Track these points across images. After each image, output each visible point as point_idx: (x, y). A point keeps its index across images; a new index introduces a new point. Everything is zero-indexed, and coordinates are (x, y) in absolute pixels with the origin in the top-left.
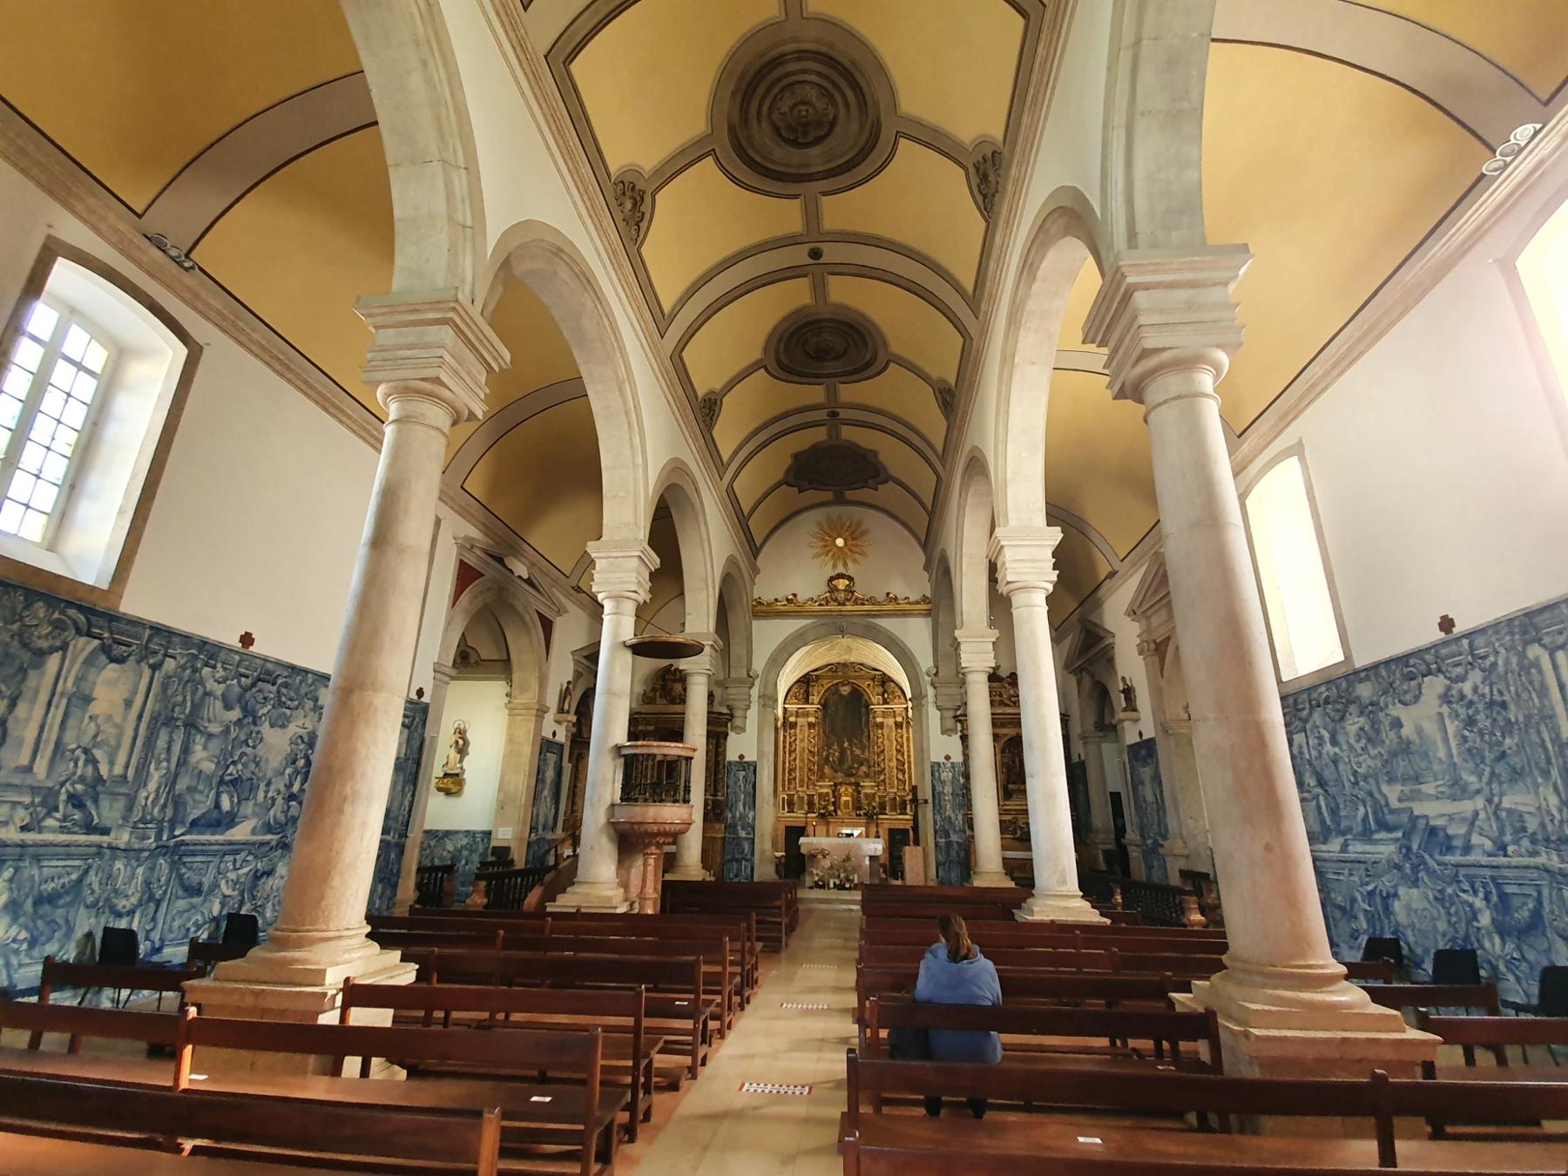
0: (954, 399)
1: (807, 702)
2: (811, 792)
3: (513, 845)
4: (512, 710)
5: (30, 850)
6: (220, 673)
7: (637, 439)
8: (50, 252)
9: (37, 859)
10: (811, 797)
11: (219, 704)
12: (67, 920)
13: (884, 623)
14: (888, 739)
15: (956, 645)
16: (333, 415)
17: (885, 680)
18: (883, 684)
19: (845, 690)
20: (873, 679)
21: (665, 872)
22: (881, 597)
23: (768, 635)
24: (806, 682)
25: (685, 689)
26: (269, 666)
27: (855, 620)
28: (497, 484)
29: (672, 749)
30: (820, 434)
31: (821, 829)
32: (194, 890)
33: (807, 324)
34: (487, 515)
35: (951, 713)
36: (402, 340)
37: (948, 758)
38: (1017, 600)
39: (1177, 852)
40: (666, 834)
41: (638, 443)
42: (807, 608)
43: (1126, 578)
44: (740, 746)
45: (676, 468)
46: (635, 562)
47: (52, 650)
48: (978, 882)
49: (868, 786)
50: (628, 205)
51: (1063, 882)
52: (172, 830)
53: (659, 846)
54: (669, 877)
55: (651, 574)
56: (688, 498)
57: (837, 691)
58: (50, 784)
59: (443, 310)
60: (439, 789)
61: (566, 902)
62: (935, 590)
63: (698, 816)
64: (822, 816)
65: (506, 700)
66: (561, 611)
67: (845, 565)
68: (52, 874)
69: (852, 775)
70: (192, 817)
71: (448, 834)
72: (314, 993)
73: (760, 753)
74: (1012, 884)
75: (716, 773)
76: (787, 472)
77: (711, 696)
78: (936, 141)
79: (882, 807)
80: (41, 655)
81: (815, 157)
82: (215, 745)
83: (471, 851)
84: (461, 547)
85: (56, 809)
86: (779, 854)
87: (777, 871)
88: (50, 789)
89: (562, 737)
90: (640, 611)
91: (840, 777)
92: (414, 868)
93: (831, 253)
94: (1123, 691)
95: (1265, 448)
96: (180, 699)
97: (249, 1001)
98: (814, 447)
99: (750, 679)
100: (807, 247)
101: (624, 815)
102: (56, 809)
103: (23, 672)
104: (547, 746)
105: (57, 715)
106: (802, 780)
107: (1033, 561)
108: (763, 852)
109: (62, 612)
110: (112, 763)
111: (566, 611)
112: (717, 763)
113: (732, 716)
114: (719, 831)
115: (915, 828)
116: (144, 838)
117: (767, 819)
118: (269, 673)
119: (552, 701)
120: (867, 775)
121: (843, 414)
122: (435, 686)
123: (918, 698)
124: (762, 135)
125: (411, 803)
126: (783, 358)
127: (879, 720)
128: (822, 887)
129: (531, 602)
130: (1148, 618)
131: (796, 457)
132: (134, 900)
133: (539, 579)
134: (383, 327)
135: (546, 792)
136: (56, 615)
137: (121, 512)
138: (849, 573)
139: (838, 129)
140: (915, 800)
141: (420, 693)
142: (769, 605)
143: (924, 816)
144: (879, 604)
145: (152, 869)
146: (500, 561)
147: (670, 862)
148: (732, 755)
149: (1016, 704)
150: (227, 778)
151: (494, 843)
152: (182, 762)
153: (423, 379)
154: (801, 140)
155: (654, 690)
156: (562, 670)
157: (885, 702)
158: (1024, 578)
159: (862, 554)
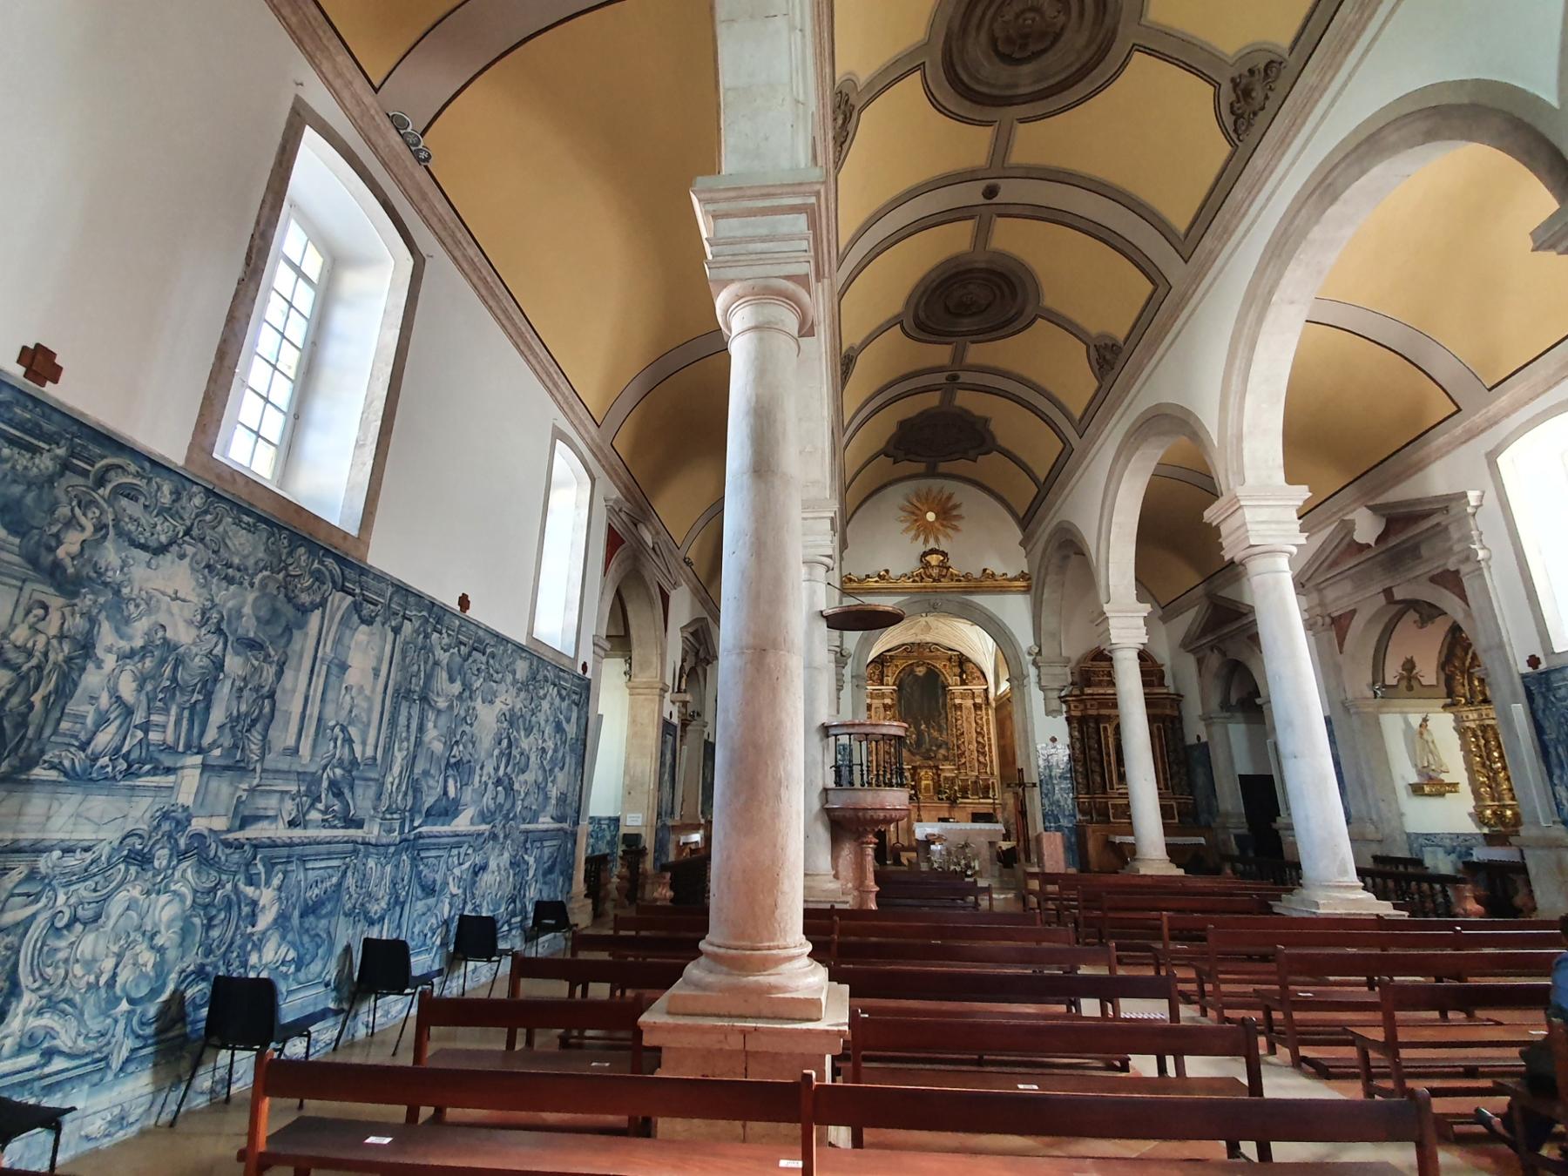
3: (643, 832)
4: (633, 691)
5: (298, 850)
6: (446, 640)
8: (300, 117)
9: (303, 860)
11: (445, 675)
12: (329, 933)
16: (522, 353)
17: (962, 661)
19: (920, 671)
20: (950, 659)
22: (977, 574)
26: (481, 633)
27: (950, 597)
28: (640, 443)
30: (933, 400)
32: (430, 890)
33: (957, 274)
35: (1055, 694)
36: (750, 232)
39: (1370, 837)
42: (900, 585)
47: (315, 606)
49: (948, 770)
50: (840, 122)
52: (412, 821)
57: (912, 671)
58: (312, 769)
59: (804, 194)
66: (675, 585)
67: (937, 540)
68: (313, 877)
69: (930, 758)
70: (427, 806)
72: (809, 1031)
78: (1184, 55)
80: (304, 611)
81: (1026, 77)
82: (443, 720)
85: (318, 799)
88: (314, 774)
89: (675, 720)
91: (918, 761)
93: (1010, 191)
96: (415, 668)
97: (735, 1043)
98: (922, 414)
100: (982, 185)
102: (318, 799)
103: (288, 630)
105: (319, 683)
107: (1278, 522)
109: (321, 562)
110: (364, 743)
116: (391, 831)
118: (480, 640)
120: (946, 758)
121: (965, 377)
122: (595, 661)
124: (977, 49)
126: (922, 315)
127: (958, 701)
130: (1320, 591)
131: (903, 424)
132: (383, 904)
134: (727, 215)
136: (316, 565)
137: (359, 445)
139: (1060, 45)
142: (860, 581)
143: (1032, 799)
145: (397, 866)
149: (1112, 684)
150: (453, 760)
151: (623, 830)
152: (419, 743)
153: (787, 278)
154: (1017, 55)
157: (963, 682)
158: (1269, 541)
159: (956, 528)
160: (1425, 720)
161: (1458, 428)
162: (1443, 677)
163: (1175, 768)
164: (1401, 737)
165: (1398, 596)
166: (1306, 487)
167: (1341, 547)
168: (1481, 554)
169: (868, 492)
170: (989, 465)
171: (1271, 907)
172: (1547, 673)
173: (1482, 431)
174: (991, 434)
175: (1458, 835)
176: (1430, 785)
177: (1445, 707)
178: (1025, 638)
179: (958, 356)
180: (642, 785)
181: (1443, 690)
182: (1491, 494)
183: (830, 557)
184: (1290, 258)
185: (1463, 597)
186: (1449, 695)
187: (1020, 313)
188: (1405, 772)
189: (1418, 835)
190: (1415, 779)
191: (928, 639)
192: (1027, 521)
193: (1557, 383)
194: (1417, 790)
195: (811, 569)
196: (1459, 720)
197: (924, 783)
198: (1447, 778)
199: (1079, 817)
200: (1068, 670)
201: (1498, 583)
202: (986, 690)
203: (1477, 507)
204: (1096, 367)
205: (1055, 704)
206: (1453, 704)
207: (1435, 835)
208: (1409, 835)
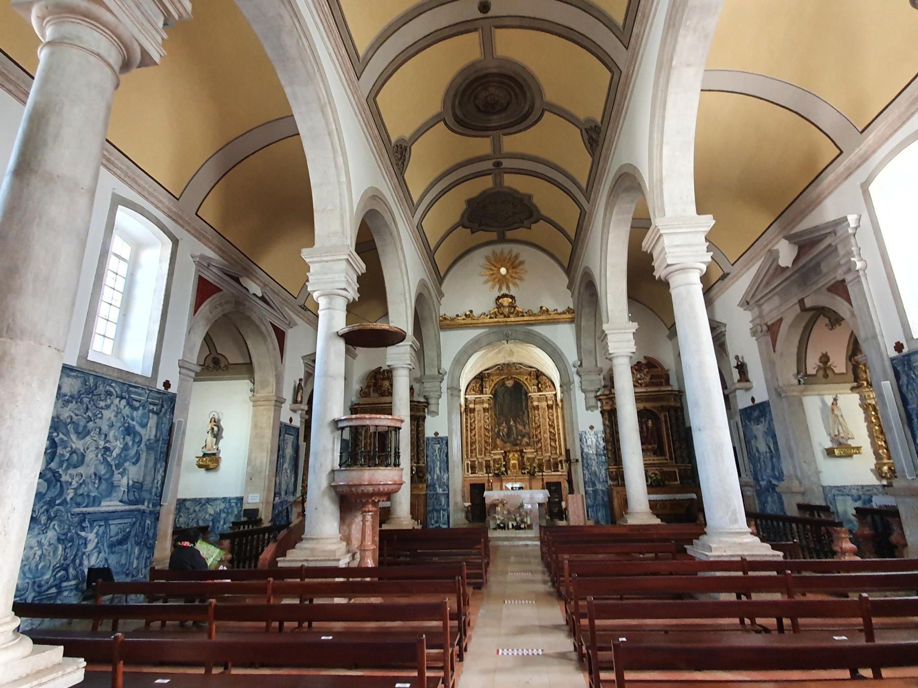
0: (597, 137)
1: (482, 393)
2: (488, 458)
4: (255, 402)
7: (340, 160)
10: (487, 462)
13: (538, 329)
14: (542, 418)
15: (604, 336)
18: (537, 377)
19: (510, 383)
20: (530, 374)
21: (382, 522)
22: (536, 310)
23: (452, 343)
24: (480, 379)
25: (391, 385)
27: (517, 328)
29: (383, 421)
30: (487, 183)
31: (496, 485)
34: (220, 239)
35: (593, 394)
37: (592, 428)
38: (673, 282)
39: (794, 490)
40: (380, 494)
41: (341, 173)
42: (480, 321)
43: (738, 276)
44: (434, 426)
45: (374, 196)
46: (344, 265)
48: (632, 521)
49: (529, 452)
51: (736, 521)
53: (375, 504)
54: (385, 527)
55: (358, 277)
56: (386, 225)
57: (503, 384)
60: (200, 466)
61: (295, 557)
62: (579, 302)
63: (407, 478)
64: (497, 475)
65: (251, 394)
66: (291, 324)
67: (508, 288)
69: (516, 445)
71: (209, 501)
72: (815, 572)
73: (450, 430)
74: (658, 521)
75: (418, 446)
76: (462, 216)
77: (411, 389)
79: (540, 466)
83: (228, 513)
84: (199, 264)
86: (467, 504)
87: (467, 517)
90: (351, 307)
91: (508, 447)
92: (170, 531)
94: (737, 367)
95: (891, 135)
98: (481, 194)
99: (440, 375)
101: (345, 478)
104: (285, 429)
106: (480, 450)
107: (690, 245)
108: (456, 504)
111: (296, 324)
112: (418, 439)
113: (428, 403)
114: (422, 489)
115: (570, 481)
117: (457, 479)
119: (288, 394)
120: (528, 444)
121: (506, 163)
122: (181, 380)
123: (566, 385)
125: (164, 477)
126: (459, 113)
127: (535, 403)
128: (504, 528)
129: (265, 316)
130: (760, 306)
131: (469, 202)
133: (270, 296)
135: (286, 466)
138: (512, 293)
140: (568, 460)
141: (167, 385)
142: (452, 319)
144: (535, 315)
146: (237, 280)
147: (385, 515)
148: (429, 433)
155: (368, 387)
156: (293, 372)
157: (539, 390)
159: (521, 279)
160: (835, 400)
161: (840, 167)
162: (851, 367)
163: (677, 444)
164: (818, 412)
165: (809, 303)
166: (711, 216)
167: (771, 271)
168: (859, 265)
169: (458, 255)
170: (540, 230)
171: (685, 550)
172: (908, 355)
173: (859, 166)
174: (535, 206)
175: (863, 487)
176: (841, 449)
177: (852, 389)
178: (571, 356)
179: (497, 146)
180: (260, 473)
181: (851, 376)
182: (865, 219)
183: (345, 289)
184: (680, 25)
185: (849, 301)
186: (855, 381)
187: (532, 107)
188: (821, 439)
189: (831, 488)
190: (829, 445)
191: (514, 360)
192: (569, 270)
193: (908, 119)
194: (830, 453)
195: (331, 299)
196: (863, 398)
197: (512, 462)
198: (852, 443)
199: (610, 482)
200: (601, 377)
201: (872, 287)
202: (555, 395)
203: (856, 228)
204: (589, 146)
205: (593, 402)
206: (858, 387)
207: (844, 487)
208: (824, 487)
